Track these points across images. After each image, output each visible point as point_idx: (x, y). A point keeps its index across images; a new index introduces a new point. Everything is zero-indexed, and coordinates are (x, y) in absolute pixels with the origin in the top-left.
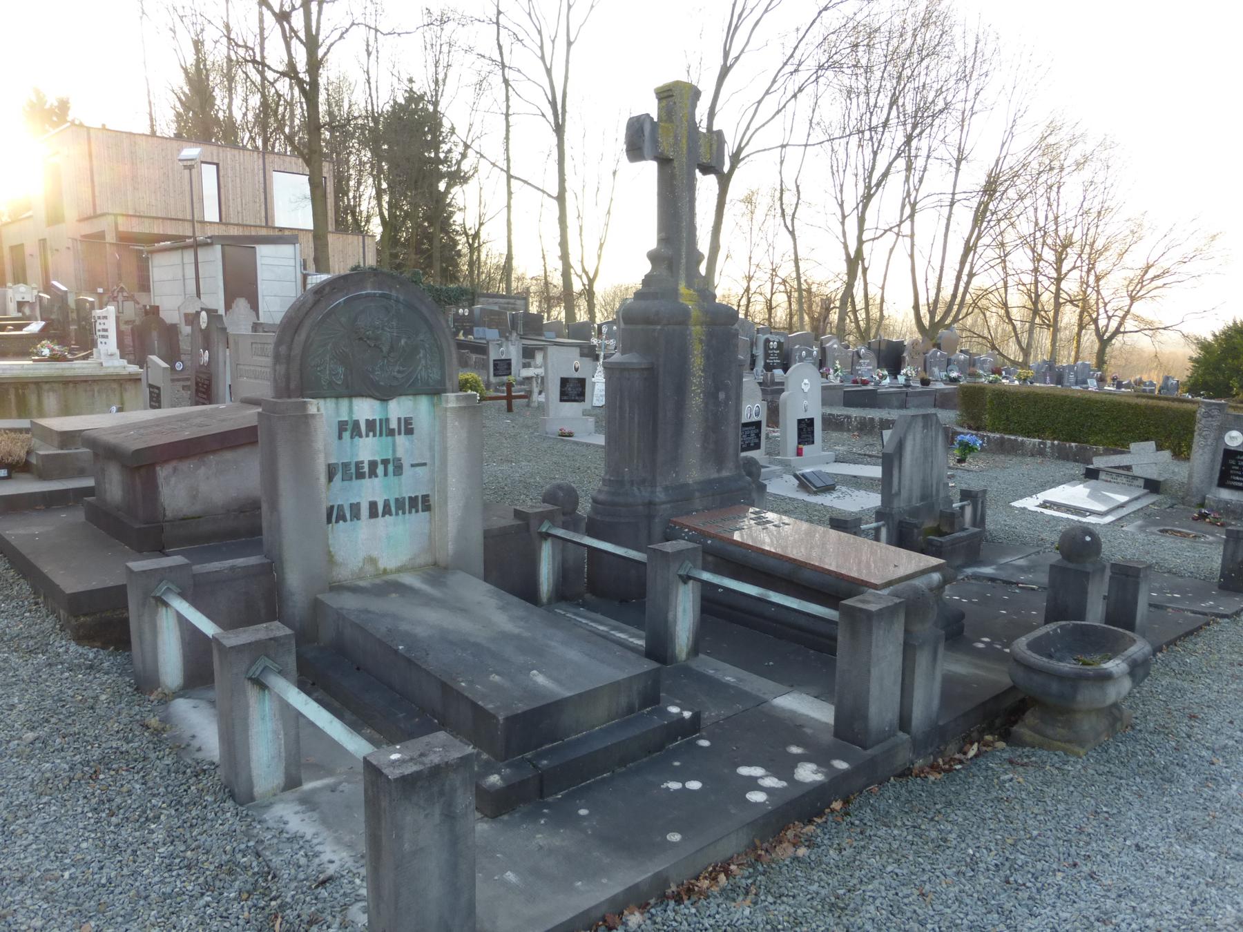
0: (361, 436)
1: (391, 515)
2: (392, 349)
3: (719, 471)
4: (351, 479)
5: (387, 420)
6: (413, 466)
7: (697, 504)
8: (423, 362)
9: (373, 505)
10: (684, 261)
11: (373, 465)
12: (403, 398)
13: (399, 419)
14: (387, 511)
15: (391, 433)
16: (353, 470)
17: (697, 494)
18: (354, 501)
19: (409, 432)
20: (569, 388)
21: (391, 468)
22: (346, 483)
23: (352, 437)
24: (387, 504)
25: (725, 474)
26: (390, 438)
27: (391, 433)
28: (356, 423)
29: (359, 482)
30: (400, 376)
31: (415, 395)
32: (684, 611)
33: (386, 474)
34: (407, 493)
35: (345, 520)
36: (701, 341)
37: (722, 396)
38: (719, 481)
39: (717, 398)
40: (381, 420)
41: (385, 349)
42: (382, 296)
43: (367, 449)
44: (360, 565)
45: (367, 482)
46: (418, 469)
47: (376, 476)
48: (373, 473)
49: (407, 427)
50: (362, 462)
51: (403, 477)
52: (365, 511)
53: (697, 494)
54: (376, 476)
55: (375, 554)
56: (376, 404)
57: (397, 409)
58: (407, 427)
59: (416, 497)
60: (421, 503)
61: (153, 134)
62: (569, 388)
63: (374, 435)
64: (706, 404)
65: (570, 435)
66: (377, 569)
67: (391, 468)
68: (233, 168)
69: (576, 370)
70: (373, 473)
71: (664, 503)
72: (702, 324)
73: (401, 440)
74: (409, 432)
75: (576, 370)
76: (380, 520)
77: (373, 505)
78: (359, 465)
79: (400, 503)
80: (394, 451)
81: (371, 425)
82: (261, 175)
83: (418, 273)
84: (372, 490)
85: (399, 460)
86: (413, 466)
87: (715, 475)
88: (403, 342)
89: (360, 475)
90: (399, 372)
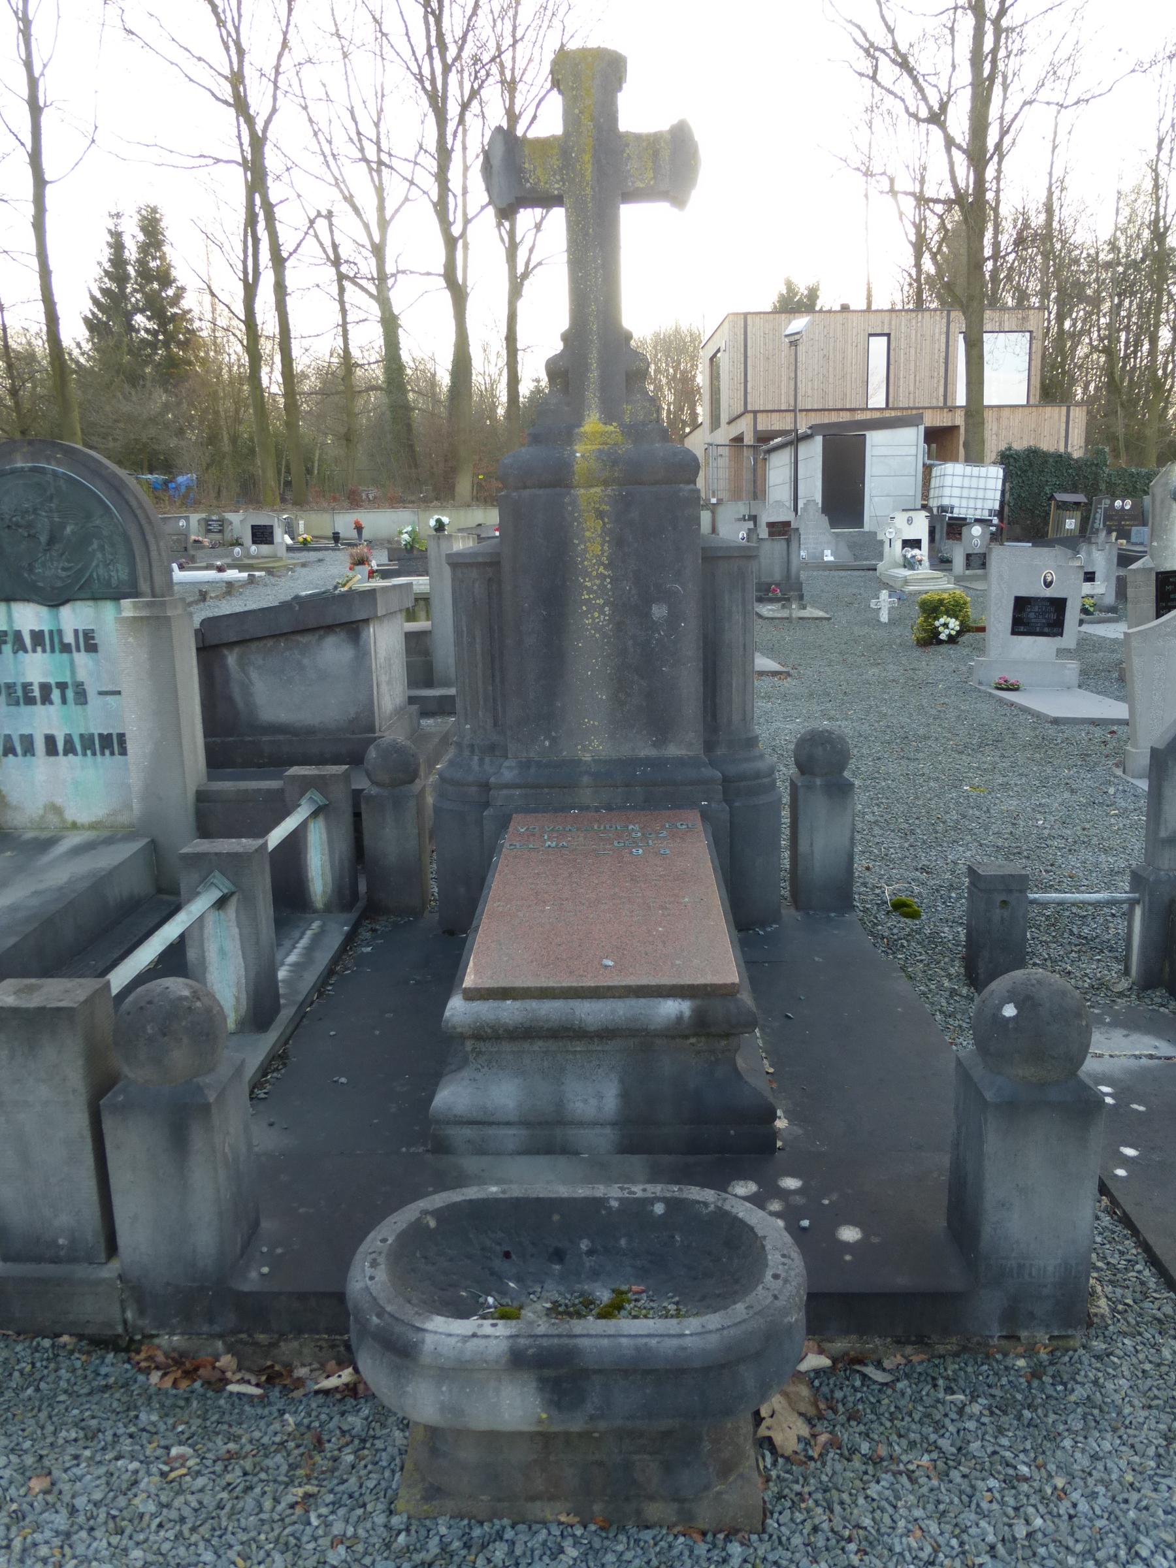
0: (26, 651)
1: (76, 754)
2: (52, 541)
3: (661, 742)
4: (35, 703)
5: (60, 632)
6: (100, 693)
7: (586, 795)
8: (99, 555)
9: (50, 741)
10: (594, 375)
11: (45, 688)
12: (79, 603)
13: (76, 632)
14: (70, 749)
15: (66, 648)
16: (20, 693)
17: (586, 779)
18: (26, 731)
19: (92, 648)
20: (1031, 614)
21: (70, 694)
22: (13, 708)
23: (15, 652)
24: (69, 740)
25: (673, 750)
26: (65, 655)
27: (66, 648)
28: (18, 635)
29: (29, 707)
30: (64, 574)
31: (94, 598)
32: (222, 952)
33: (64, 701)
34: (96, 729)
35: (15, 755)
36: (600, 515)
37: (659, 611)
38: (656, 764)
39: (647, 615)
40: (51, 632)
41: (43, 539)
42: (34, 470)
43: (36, 668)
44: (41, 812)
45: (39, 709)
46: (109, 698)
47: (51, 703)
48: (46, 699)
49: (88, 641)
50: (31, 684)
51: (89, 707)
52: (40, 745)
53: (586, 779)
54: (51, 703)
55: (59, 801)
56: (43, 611)
57: (73, 618)
58: (88, 641)
59: (110, 735)
60: (111, 744)
61: (869, 309)
62: (1031, 614)
63: (44, 651)
64: (619, 627)
65: (1014, 688)
66: (64, 821)
67: (70, 694)
68: (908, 337)
69: (1048, 584)
70: (46, 699)
71: (506, 786)
72: (606, 483)
73: (82, 659)
74: (92, 648)
75: (1048, 584)
76: (61, 759)
77: (50, 741)
78: (26, 687)
79: (88, 742)
80: (73, 672)
81: (38, 637)
82: (943, 340)
83: (1102, 452)
84: (47, 720)
85: (82, 684)
86: (100, 693)
87: (646, 751)
88: (69, 529)
89: (30, 701)
90: (64, 569)
